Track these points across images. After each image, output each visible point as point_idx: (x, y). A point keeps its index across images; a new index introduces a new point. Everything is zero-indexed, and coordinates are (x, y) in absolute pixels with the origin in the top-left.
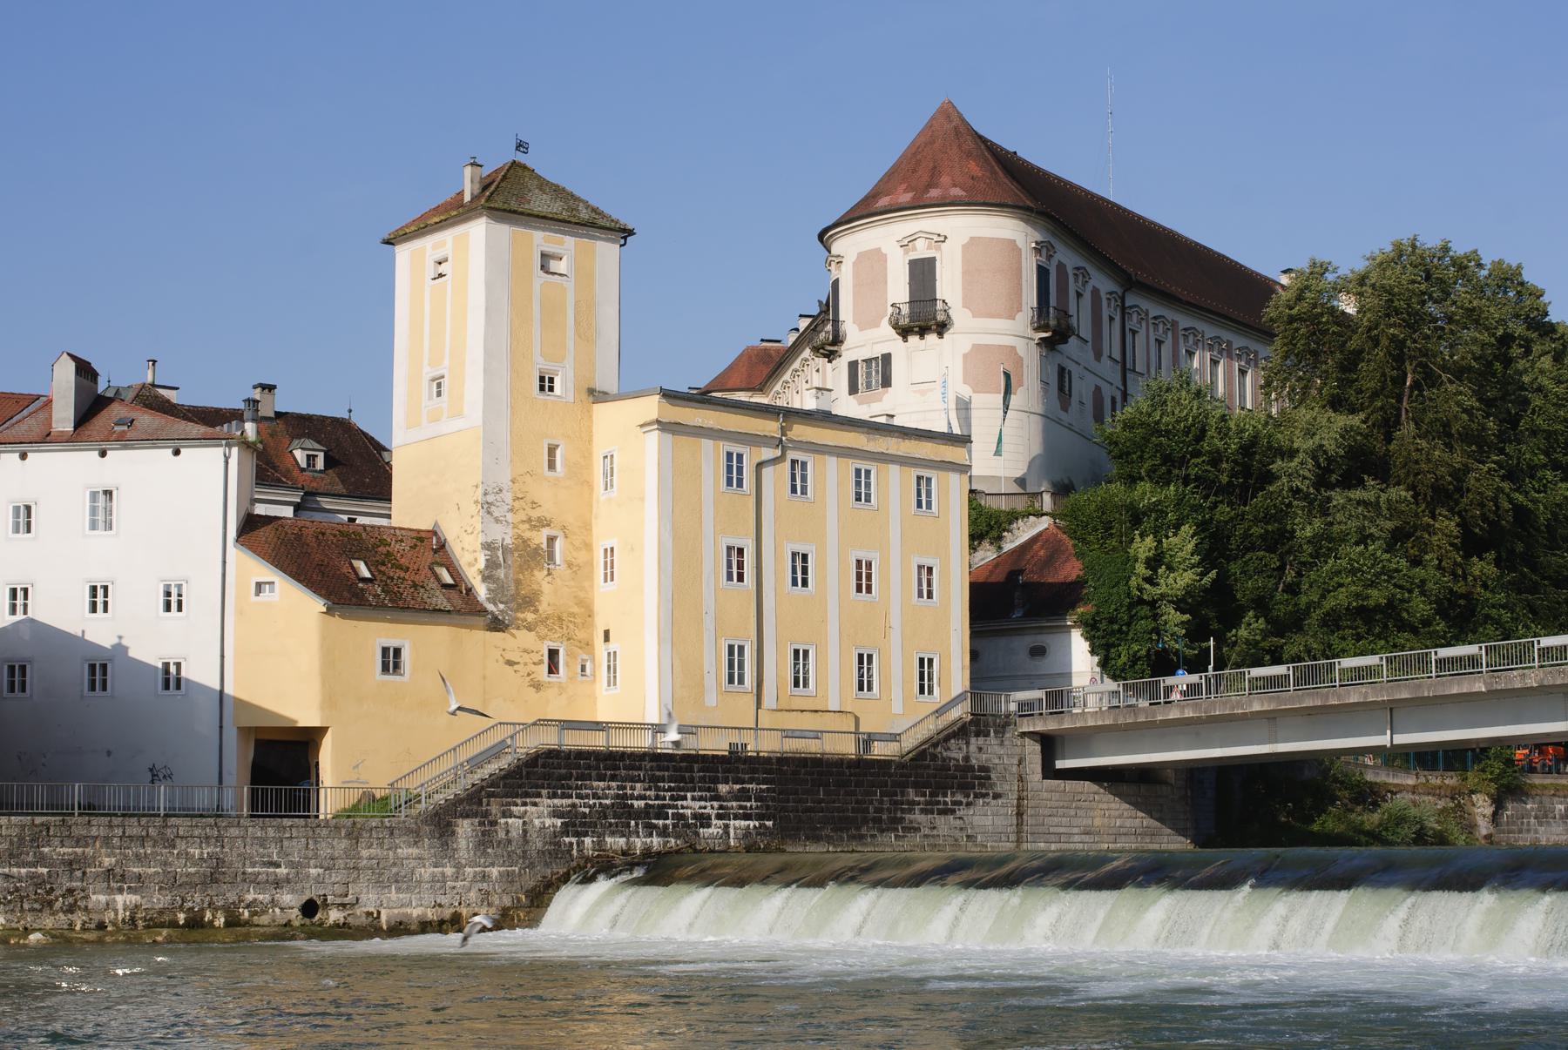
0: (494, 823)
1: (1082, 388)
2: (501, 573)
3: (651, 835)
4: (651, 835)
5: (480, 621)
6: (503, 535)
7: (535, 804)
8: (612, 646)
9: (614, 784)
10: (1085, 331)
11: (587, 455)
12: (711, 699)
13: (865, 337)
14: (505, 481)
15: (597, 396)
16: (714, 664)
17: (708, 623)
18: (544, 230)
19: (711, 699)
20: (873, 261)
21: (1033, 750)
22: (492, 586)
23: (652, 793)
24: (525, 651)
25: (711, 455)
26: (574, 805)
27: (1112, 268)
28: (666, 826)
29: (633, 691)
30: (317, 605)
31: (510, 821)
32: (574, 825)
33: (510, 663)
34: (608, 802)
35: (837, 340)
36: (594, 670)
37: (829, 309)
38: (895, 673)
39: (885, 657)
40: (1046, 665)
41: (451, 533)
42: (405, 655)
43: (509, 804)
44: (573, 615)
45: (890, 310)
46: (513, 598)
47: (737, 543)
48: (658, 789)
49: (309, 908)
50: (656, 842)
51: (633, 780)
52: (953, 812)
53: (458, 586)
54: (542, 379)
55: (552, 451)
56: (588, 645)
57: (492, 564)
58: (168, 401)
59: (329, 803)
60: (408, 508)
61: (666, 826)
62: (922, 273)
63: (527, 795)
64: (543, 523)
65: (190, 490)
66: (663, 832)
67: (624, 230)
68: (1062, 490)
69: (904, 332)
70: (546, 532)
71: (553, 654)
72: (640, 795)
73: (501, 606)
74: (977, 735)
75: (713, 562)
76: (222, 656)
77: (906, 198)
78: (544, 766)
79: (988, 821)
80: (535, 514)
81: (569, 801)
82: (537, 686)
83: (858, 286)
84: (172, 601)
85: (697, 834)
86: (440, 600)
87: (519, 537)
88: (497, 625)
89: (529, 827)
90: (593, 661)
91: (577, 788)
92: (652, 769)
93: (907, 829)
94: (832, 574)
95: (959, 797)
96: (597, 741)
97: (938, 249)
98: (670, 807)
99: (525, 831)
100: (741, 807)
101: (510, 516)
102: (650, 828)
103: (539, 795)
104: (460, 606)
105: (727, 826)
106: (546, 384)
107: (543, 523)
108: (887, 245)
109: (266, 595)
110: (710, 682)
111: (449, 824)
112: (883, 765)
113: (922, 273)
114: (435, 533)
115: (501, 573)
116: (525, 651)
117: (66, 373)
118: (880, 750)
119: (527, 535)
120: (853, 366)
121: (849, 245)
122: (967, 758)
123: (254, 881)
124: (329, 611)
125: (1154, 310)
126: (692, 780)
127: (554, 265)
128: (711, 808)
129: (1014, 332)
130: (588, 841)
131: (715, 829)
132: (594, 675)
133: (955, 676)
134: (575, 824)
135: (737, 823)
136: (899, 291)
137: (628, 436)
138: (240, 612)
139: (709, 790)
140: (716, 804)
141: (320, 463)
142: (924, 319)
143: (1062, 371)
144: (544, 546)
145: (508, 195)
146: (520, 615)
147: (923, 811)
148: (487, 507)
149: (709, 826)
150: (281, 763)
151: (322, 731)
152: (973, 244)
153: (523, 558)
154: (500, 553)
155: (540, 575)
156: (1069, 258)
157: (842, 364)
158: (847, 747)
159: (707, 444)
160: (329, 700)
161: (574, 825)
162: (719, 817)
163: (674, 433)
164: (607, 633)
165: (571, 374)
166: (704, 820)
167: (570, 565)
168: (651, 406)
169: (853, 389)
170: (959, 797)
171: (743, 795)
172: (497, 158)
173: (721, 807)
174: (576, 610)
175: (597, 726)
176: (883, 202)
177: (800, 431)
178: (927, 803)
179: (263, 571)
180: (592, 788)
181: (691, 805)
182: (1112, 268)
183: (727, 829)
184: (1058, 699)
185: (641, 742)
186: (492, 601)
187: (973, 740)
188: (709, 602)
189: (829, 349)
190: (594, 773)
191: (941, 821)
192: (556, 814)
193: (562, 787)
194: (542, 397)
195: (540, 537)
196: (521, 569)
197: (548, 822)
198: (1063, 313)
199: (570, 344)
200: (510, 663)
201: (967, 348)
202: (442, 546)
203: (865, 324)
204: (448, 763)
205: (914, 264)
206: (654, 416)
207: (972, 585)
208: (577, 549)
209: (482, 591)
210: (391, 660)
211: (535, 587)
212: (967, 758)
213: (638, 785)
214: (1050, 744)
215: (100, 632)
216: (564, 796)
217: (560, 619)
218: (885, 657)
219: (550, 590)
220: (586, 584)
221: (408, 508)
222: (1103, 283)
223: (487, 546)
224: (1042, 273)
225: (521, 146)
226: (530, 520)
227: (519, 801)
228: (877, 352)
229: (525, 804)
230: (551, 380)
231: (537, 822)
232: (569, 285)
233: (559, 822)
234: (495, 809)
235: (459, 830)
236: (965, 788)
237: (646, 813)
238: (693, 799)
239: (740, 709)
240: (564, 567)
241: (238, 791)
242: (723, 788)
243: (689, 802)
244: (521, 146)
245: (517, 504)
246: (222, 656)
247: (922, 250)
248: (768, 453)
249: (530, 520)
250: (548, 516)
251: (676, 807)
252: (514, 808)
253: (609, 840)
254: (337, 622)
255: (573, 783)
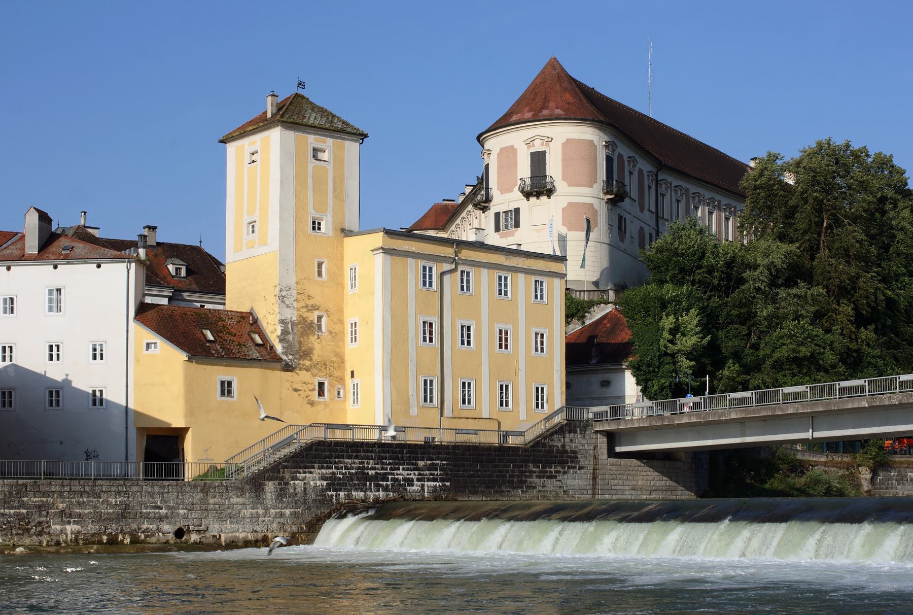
0: (287, 484)
1: (632, 228)
2: (290, 337)
3: (379, 491)
4: (379, 491)
5: (278, 365)
6: (292, 315)
7: (311, 473)
8: (356, 380)
9: (357, 461)
10: (634, 194)
11: (341, 268)
12: (414, 411)
13: (504, 199)
14: (292, 281)
15: (346, 233)
16: (415, 391)
17: (412, 367)
18: (314, 134)
19: (414, 411)
20: (509, 153)
21: (602, 441)
22: (285, 345)
23: (379, 466)
24: (305, 383)
25: (413, 267)
26: (333, 473)
27: (650, 159)
28: (387, 486)
29: (367, 406)
30: (183, 356)
31: (296, 482)
32: (334, 485)
33: (296, 390)
34: (353, 471)
35: (488, 200)
36: (345, 394)
37: (482, 182)
38: (522, 395)
39: (516, 385)
40: (611, 391)
41: (260, 314)
42: (234, 385)
43: (295, 473)
44: (332, 362)
45: (519, 182)
46: (298, 352)
47: (429, 320)
48: (383, 464)
49: (179, 533)
50: (381, 494)
51: (368, 458)
52: (555, 477)
53: (266, 346)
54: (314, 223)
55: (320, 265)
56: (341, 380)
57: (285, 332)
58: (93, 236)
59: (190, 472)
60: (235, 299)
61: (387, 486)
62: (538, 160)
63: (306, 467)
64: (315, 308)
65: (110, 286)
66: (386, 489)
67: (362, 135)
68: (620, 289)
69: (527, 195)
70: (317, 313)
71: (321, 385)
72: (372, 468)
73: (291, 357)
74: (570, 432)
75: (414, 330)
76: (127, 386)
77: (529, 115)
78: (316, 450)
79: (576, 482)
80: (310, 303)
81: (331, 471)
82: (312, 404)
83: (500, 167)
84: (97, 354)
85: (406, 490)
86: (255, 354)
87: (301, 316)
88: (288, 368)
89: (307, 486)
90: (344, 389)
91: (336, 463)
92: (379, 452)
93: (528, 487)
94: (484, 338)
95: (559, 469)
96: (347, 436)
97: (548, 145)
98: (390, 474)
99: (305, 488)
100: (431, 474)
101: (295, 304)
102: (378, 487)
103: (313, 468)
104: (267, 357)
105: (423, 485)
106: (316, 226)
107: (315, 308)
108: (519, 141)
109: (152, 350)
110: (413, 401)
111: (261, 484)
112: (515, 450)
113: (538, 160)
114: (251, 314)
115: (290, 337)
116: (305, 383)
117: (33, 220)
118: (512, 441)
119: (305, 315)
120: (497, 215)
121: (494, 143)
122: (563, 446)
123: (147, 517)
124: (190, 360)
125: (675, 182)
126: (403, 459)
127: (320, 155)
128: (414, 475)
129: (591, 195)
130: (342, 494)
131: (416, 487)
132: (345, 397)
133: (557, 397)
134: (334, 484)
135: (429, 483)
136: (524, 171)
137: (365, 261)
138: (137, 360)
139: (412, 464)
140: (417, 473)
141: (183, 273)
142: (539, 187)
143: (620, 218)
144: (316, 321)
145: (293, 113)
146: (302, 362)
147: (537, 477)
148: (282, 298)
149: (413, 485)
150: (162, 448)
151: (185, 430)
152: (568, 143)
153: (303, 329)
154: (289, 326)
155: (313, 338)
156: (624, 151)
157: (491, 214)
158: (493, 439)
159: (411, 261)
160: (190, 412)
161: (334, 485)
162: (418, 480)
163: (391, 254)
164: (352, 372)
165: (331, 219)
166: (410, 482)
167: (331, 333)
168: (378, 239)
169: (497, 229)
170: (559, 469)
171: (433, 467)
172: (286, 92)
173: (419, 474)
174: (334, 359)
175: (347, 427)
176: (515, 118)
177: (466, 254)
178: (540, 472)
179: (150, 336)
180: (344, 463)
181: (402, 473)
182: (650, 159)
183: (423, 487)
184: (618, 411)
185: (373, 436)
186: (285, 353)
187: (567, 435)
188: (412, 353)
189: (483, 205)
190: (345, 454)
191: (548, 482)
192: (323, 478)
193: (327, 463)
194: (313, 233)
195: (313, 316)
196: (302, 335)
197: (318, 483)
198: (621, 184)
199: (330, 202)
200: (296, 390)
201: (565, 205)
202: (256, 321)
203: (504, 190)
204: (260, 449)
205: (533, 155)
206: (380, 245)
207: (566, 344)
208: (335, 323)
209: (279, 348)
210: (226, 389)
211: (310, 345)
212: (563, 446)
213: (371, 461)
214: (612, 438)
215: (55, 372)
216: (328, 468)
217: (325, 364)
218: (516, 385)
219: (319, 347)
220: (340, 344)
221: (235, 299)
222: (645, 166)
223: (282, 322)
224: (609, 160)
225: (301, 84)
226: (307, 306)
227: (301, 471)
228: (512, 207)
229: (305, 473)
230: (319, 224)
231: (312, 483)
232: (330, 167)
233: (325, 483)
234: (287, 476)
235: (267, 488)
236: (562, 463)
237: (376, 477)
238: (403, 469)
239: (431, 417)
240: (327, 334)
241: (137, 465)
242: (421, 463)
243: (401, 471)
244: (301, 84)
245: (299, 297)
246: (127, 386)
247: (538, 147)
248: (447, 267)
249: (307, 306)
250: (318, 304)
251: (393, 474)
252: (298, 475)
253: (354, 493)
254: (194, 366)
255: (333, 460)
